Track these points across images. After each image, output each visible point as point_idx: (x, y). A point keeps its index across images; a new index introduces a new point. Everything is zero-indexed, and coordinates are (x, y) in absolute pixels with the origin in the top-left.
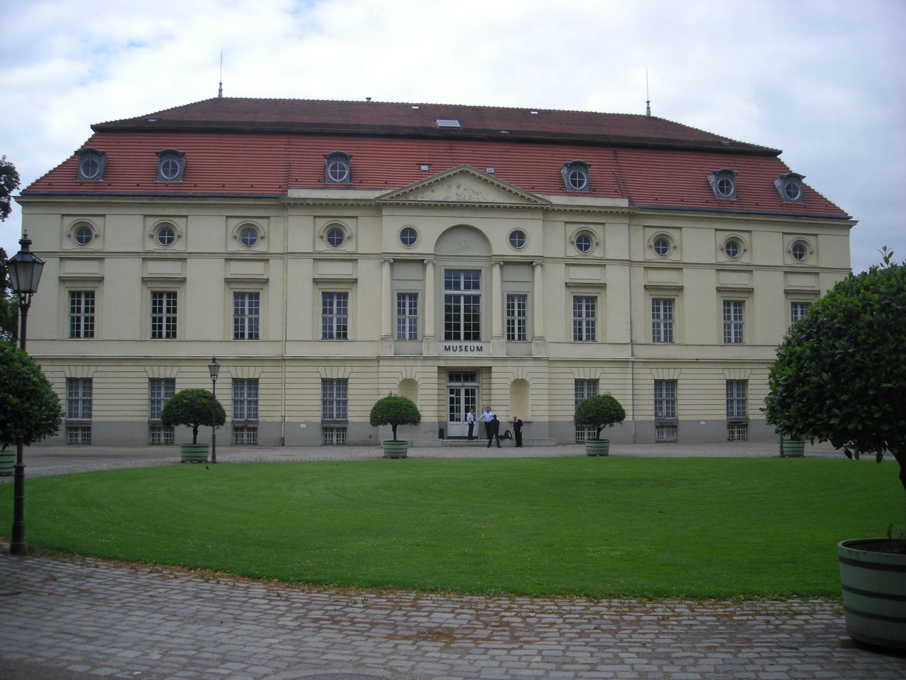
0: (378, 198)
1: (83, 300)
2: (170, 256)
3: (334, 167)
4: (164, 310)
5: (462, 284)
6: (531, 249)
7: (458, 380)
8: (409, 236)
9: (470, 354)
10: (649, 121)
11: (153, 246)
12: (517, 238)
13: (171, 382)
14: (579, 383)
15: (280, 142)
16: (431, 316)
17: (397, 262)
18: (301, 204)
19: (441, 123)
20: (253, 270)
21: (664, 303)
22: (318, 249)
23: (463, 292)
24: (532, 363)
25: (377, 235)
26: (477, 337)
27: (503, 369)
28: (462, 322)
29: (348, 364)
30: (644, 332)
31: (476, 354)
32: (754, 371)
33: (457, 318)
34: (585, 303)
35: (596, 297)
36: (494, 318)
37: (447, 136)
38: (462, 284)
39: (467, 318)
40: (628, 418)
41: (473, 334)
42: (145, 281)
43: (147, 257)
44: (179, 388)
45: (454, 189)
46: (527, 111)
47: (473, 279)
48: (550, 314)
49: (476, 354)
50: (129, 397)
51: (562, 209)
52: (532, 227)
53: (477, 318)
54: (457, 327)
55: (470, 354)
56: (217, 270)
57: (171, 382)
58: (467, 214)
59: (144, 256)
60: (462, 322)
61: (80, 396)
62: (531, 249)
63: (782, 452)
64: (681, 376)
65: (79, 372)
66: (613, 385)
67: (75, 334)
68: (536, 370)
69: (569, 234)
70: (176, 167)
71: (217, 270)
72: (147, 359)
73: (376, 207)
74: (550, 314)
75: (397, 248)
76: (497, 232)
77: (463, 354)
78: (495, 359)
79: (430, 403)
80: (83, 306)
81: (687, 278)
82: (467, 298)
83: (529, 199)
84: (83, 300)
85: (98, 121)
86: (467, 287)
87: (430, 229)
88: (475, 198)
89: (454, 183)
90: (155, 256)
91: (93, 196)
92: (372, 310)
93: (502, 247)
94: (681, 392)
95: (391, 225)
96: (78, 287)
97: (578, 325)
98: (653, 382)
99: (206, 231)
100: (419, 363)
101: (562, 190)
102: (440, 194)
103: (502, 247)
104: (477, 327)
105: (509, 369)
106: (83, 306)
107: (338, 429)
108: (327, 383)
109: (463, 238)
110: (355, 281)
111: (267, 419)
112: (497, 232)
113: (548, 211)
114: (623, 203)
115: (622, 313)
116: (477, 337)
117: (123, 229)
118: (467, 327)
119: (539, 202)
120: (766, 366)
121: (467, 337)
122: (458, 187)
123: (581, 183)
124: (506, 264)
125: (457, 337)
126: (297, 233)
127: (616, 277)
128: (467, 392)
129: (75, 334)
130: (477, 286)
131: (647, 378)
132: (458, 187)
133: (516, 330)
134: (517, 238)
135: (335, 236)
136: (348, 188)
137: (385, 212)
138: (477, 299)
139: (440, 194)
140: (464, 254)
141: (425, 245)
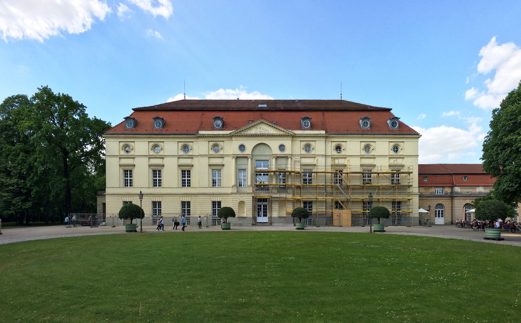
0: (230, 133)
1: (129, 173)
2: (158, 157)
3: (305, 123)
6: (288, 151)
7: (261, 201)
8: (242, 147)
10: (341, 102)
11: (181, 153)
12: (282, 147)
13: (219, 203)
14: (214, 203)
15: (199, 114)
17: (237, 158)
18: (203, 137)
19: (260, 106)
22: (210, 153)
25: (231, 147)
29: (221, 196)
37: (262, 110)
42: (150, 166)
43: (179, 157)
44: (223, 206)
45: (259, 129)
46: (251, 101)
52: (287, 143)
56: (205, 161)
57: (219, 203)
58: (263, 138)
61: (157, 208)
62: (288, 151)
63: (371, 231)
65: (157, 199)
67: (184, 185)
69: (333, 146)
71: (205, 161)
72: (151, 194)
73: (230, 136)
75: (238, 152)
76: (274, 145)
81: (137, 161)
84: (129, 173)
85: (135, 107)
87: (250, 144)
88: (266, 133)
89: (259, 127)
91: (113, 134)
93: (276, 151)
95: (236, 143)
96: (127, 168)
97: (183, 181)
99: (171, 146)
100: (246, 195)
101: (301, 128)
102: (253, 131)
103: (276, 151)
108: (183, 203)
109: (263, 148)
110: (163, 166)
113: (294, 136)
114: (323, 132)
117: (141, 146)
120: (249, 195)
122: (260, 128)
123: (308, 125)
124: (277, 158)
126: (201, 147)
128: (264, 206)
129: (184, 185)
132: (260, 128)
134: (282, 147)
136: (221, 130)
137: (233, 139)
139: (253, 131)
141: (248, 151)
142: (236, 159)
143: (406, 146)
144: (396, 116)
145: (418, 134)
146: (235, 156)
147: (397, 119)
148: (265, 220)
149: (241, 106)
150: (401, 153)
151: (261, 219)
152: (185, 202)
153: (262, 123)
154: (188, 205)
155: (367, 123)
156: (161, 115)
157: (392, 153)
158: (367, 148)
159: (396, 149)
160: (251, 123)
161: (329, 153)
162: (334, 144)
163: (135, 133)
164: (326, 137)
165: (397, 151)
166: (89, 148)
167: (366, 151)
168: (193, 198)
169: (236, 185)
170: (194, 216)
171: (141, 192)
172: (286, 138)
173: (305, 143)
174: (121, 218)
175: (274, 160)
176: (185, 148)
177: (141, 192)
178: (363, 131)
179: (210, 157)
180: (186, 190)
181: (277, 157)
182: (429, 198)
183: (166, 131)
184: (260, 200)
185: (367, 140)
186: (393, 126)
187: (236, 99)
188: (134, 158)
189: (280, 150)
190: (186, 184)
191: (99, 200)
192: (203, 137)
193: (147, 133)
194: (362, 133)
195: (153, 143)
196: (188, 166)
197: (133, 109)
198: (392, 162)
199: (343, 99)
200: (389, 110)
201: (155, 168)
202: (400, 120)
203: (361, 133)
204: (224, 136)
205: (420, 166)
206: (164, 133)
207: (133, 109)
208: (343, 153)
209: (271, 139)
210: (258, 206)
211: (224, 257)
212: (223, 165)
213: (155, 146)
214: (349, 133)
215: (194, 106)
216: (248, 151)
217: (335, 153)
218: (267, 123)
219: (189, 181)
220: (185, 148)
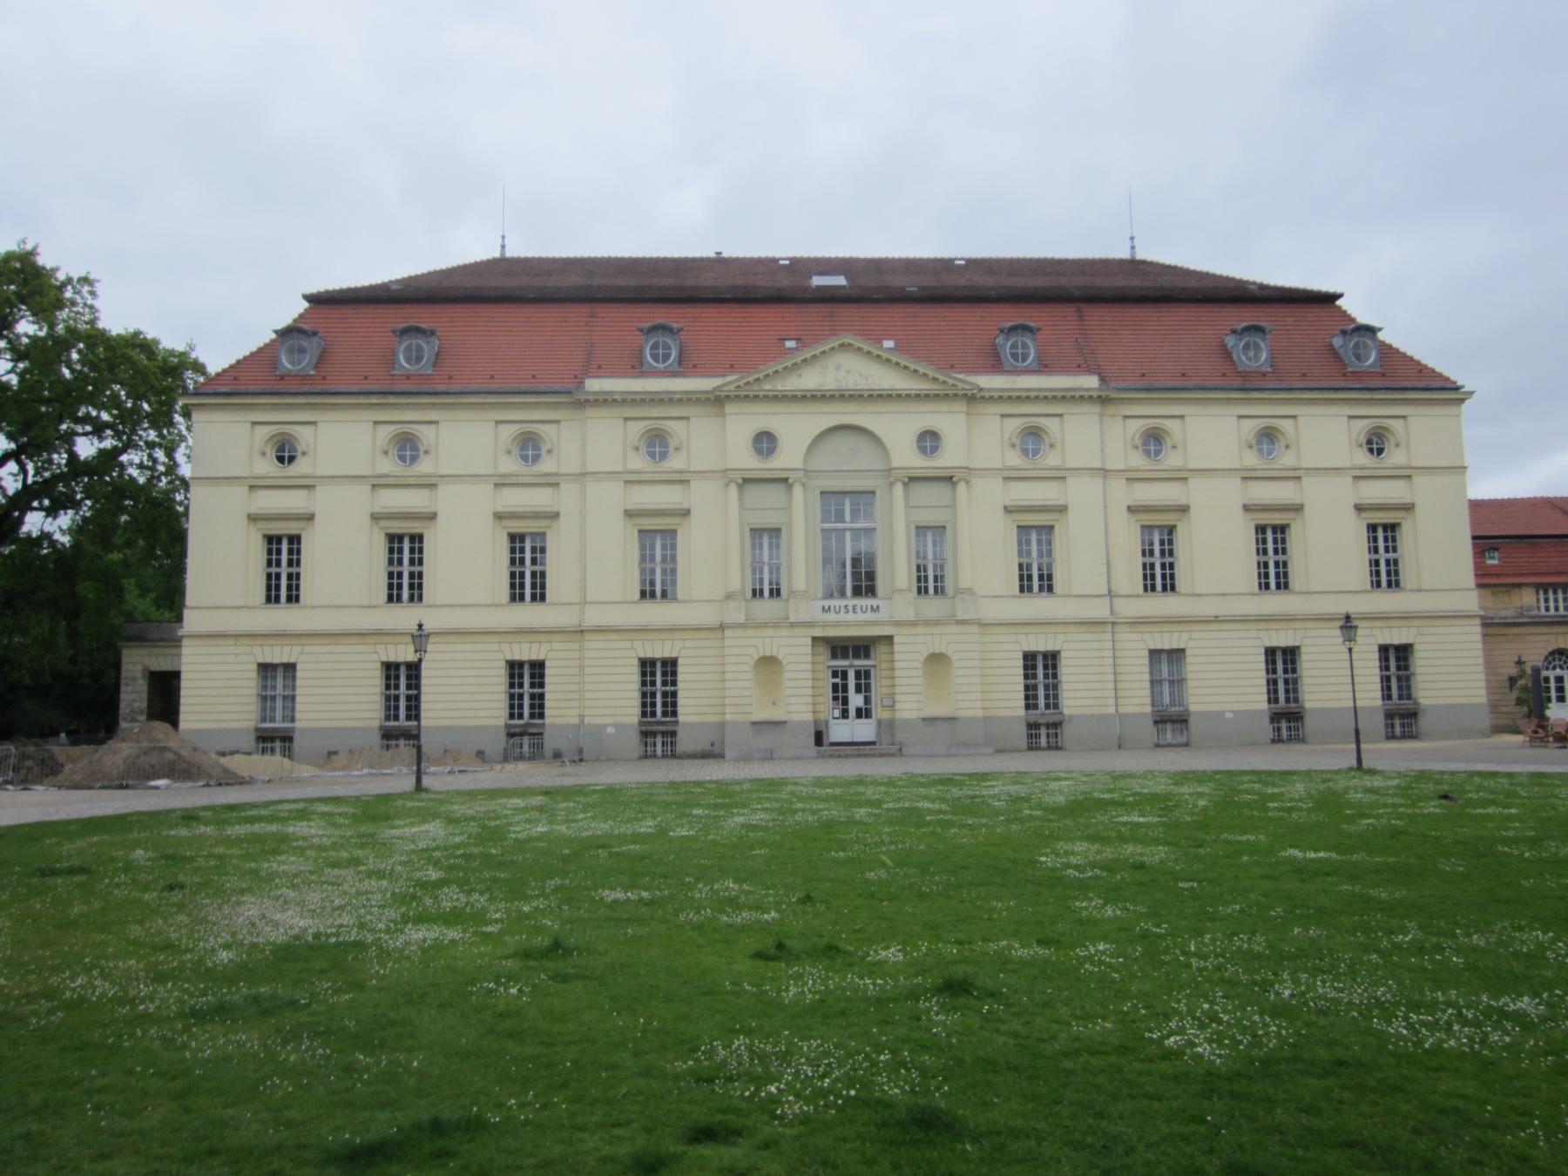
0: (718, 388)
2: (412, 481)
3: (1014, 346)
8: (765, 442)
9: (851, 617)
12: (929, 440)
16: (802, 565)
18: (605, 401)
19: (817, 281)
20: (1281, 493)
25: (717, 442)
31: (870, 616)
36: (896, 571)
48: (985, 557)
49: (870, 616)
52: (949, 421)
55: (860, 617)
56: (1234, 493)
58: (852, 407)
72: (378, 633)
73: (717, 401)
74: (985, 557)
76: (898, 430)
78: (899, 624)
87: (796, 430)
90: (390, 481)
92: (711, 559)
93: (906, 456)
94: (1193, 666)
95: (742, 423)
99: (465, 441)
102: (810, 379)
103: (906, 456)
107: (664, 734)
108: (647, 665)
109: (847, 442)
113: (974, 398)
114: (1091, 382)
117: (343, 440)
119: (960, 385)
122: (838, 368)
123: (666, 357)
126: (594, 442)
127: (1081, 495)
128: (858, 675)
132: (838, 368)
134: (929, 440)
135: (657, 444)
136: (674, 374)
137: (730, 408)
139: (810, 379)
140: (848, 465)
141: (789, 457)
143: (1418, 430)
144: (1362, 319)
145: (1457, 389)
146: (738, 477)
147: (1370, 331)
148: (863, 730)
149: (740, 281)
150: (1394, 457)
151: (841, 731)
153: (844, 347)
154: (409, 677)
156: (423, 317)
157: (1363, 458)
158: (1154, 440)
159: (1375, 444)
161: (1115, 463)
162: (1136, 426)
163: (319, 388)
164: (1104, 401)
165: (1380, 451)
166: (86, 448)
168: (556, 646)
169: (743, 592)
170: (559, 721)
171: (420, 626)
172: (944, 406)
175: (899, 488)
176: (407, 447)
177: (420, 626)
178: (1246, 375)
179: (502, 483)
182: (1516, 630)
185: (1265, 411)
186: (1358, 357)
187: (712, 255)
188: (556, 485)
189: (922, 449)
190: (528, 591)
191: (136, 663)
192: (605, 401)
193: (371, 388)
194: (1241, 384)
195: (392, 428)
196: (537, 516)
197: (308, 298)
198: (515, 499)
199: (1139, 256)
200: (1329, 299)
201: (397, 527)
202: (1381, 336)
203: (1238, 383)
204: (687, 399)
205: (1476, 506)
206: (442, 388)
207: (308, 298)
209: (870, 408)
210: (835, 674)
211: (610, 896)
212: (686, 513)
213: (1268, 436)
214: (1190, 384)
215: (552, 282)
219: (294, 578)
220: (529, 446)
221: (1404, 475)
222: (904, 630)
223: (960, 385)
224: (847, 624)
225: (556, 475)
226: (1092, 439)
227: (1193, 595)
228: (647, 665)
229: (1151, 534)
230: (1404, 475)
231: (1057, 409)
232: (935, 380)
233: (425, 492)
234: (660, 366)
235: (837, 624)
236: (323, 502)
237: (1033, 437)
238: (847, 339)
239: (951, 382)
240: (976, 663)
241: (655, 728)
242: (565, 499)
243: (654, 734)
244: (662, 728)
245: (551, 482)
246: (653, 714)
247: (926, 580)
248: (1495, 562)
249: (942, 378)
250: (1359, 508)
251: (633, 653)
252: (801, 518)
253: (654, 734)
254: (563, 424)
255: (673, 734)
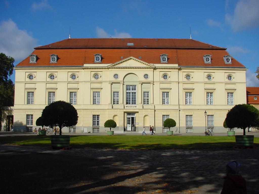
4: (146, 97)
5: (131, 89)
6: (150, 79)
8: (116, 76)
9: (133, 108)
12: (146, 76)
16: (122, 98)
20: (75, 86)
21: (210, 93)
23: (131, 91)
24: (150, 110)
25: (107, 75)
26: (135, 103)
27: (142, 112)
28: (131, 99)
30: (182, 101)
31: (135, 108)
32: (194, 112)
33: (130, 98)
34: (166, 94)
35: (192, 92)
36: (139, 98)
38: (131, 89)
39: (132, 98)
40: (177, 125)
41: (134, 102)
42: (47, 89)
47: (134, 87)
48: (156, 97)
49: (135, 108)
50: (219, 123)
51: (100, 68)
52: (150, 72)
53: (135, 98)
54: (130, 101)
55: (133, 108)
56: (88, 86)
59: (160, 82)
60: (131, 99)
62: (150, 79)
64: (194, 114)
66: (173, 116)
68: (151, 112)
70: (230, 60)
74: (156, 97)
75: (114, 80)
76: (140, 74)
77: (130, 108)
78: (139, 109)
79: (119, 122)
80: (31, 96)
82: (132, 93)
83: (149, 65)
85: (35, 47)
86: (132, 89)
87: (122, 73)
90: (49, 82)
92: (105, 97)
94: (193, 118)
98: (26, 115)
100: (119, 110)
101: (160, 63)
104: (135, 101)
105: (144, 112)
106: (31, 96)
107: (97, 128)
108: (94, 116)
111: (158, 126)
112: (140, 74)
114: (176, 65)
115: (176, 96)
116: (135, 103)
117: (41, 74)
118: (132, 101)
119: (152, 66)
121: (132, 103)
125: (130, 103)
127: (174, 86)
130: (135, 89)
131: (183, 115)
133: (146, 101)
134: (146, 76)
135: (96, 76)
138: (135, 93)
140: (130, 80)
141: (120, 79)
142: (142, 84)
150: (233, 80)
152: (95, 115)
155: (209, 59)
157: (227, 80)
159: (230, 77)
160: (126, 57)
162: (185, 74)
167: (187, 79)
173: (71, 73)
174: (105, 127)
178: (227, 65)
180: (95, 107)
181: (143, 83)
183: (61, 63)
184: (129, 113)
185: (209, 71)
189: (145, 78)
194: (206, 66)
197: (35, 49)
208: (192, 80)
216: (120, 79)
217: (185, 80)
218: (135, 59)
221: (234, 84)
222: (141, 111)
223: (152, 66)
224: (130, 109)
225: (78, 81)
226: (176, 75)
227: (193, 105)
228: (94, 116)
229: (208, 94)
230: (234, 84)
231: (170, 70)
232: (147, 65)
233: (55, 84)
234: (98, 62)
235: (129, 109)
236: (80, 86)
237: (165, 76)
238: (132, 57)
239: (150, 65)
240: (108, 117)
241: (96, 127)
242: (37, 86)
243: (95, 128)
244: (97, 127)
245: (193, 83)
246: (95, 125)
247: (147, 101)
248: (256, 99)
249: (149, 65)
250: (205, 89)
251: (91, 114)
252: (121, 89)
253: (95, 128)
254: (37, 72)
255: (99, 128)
